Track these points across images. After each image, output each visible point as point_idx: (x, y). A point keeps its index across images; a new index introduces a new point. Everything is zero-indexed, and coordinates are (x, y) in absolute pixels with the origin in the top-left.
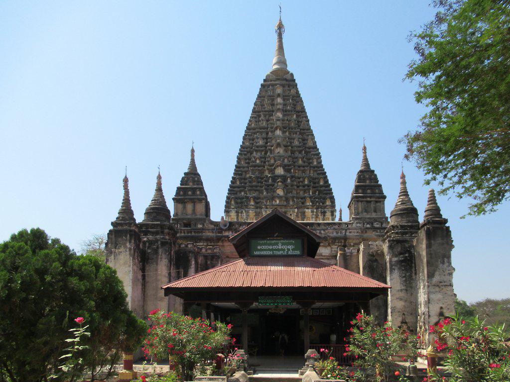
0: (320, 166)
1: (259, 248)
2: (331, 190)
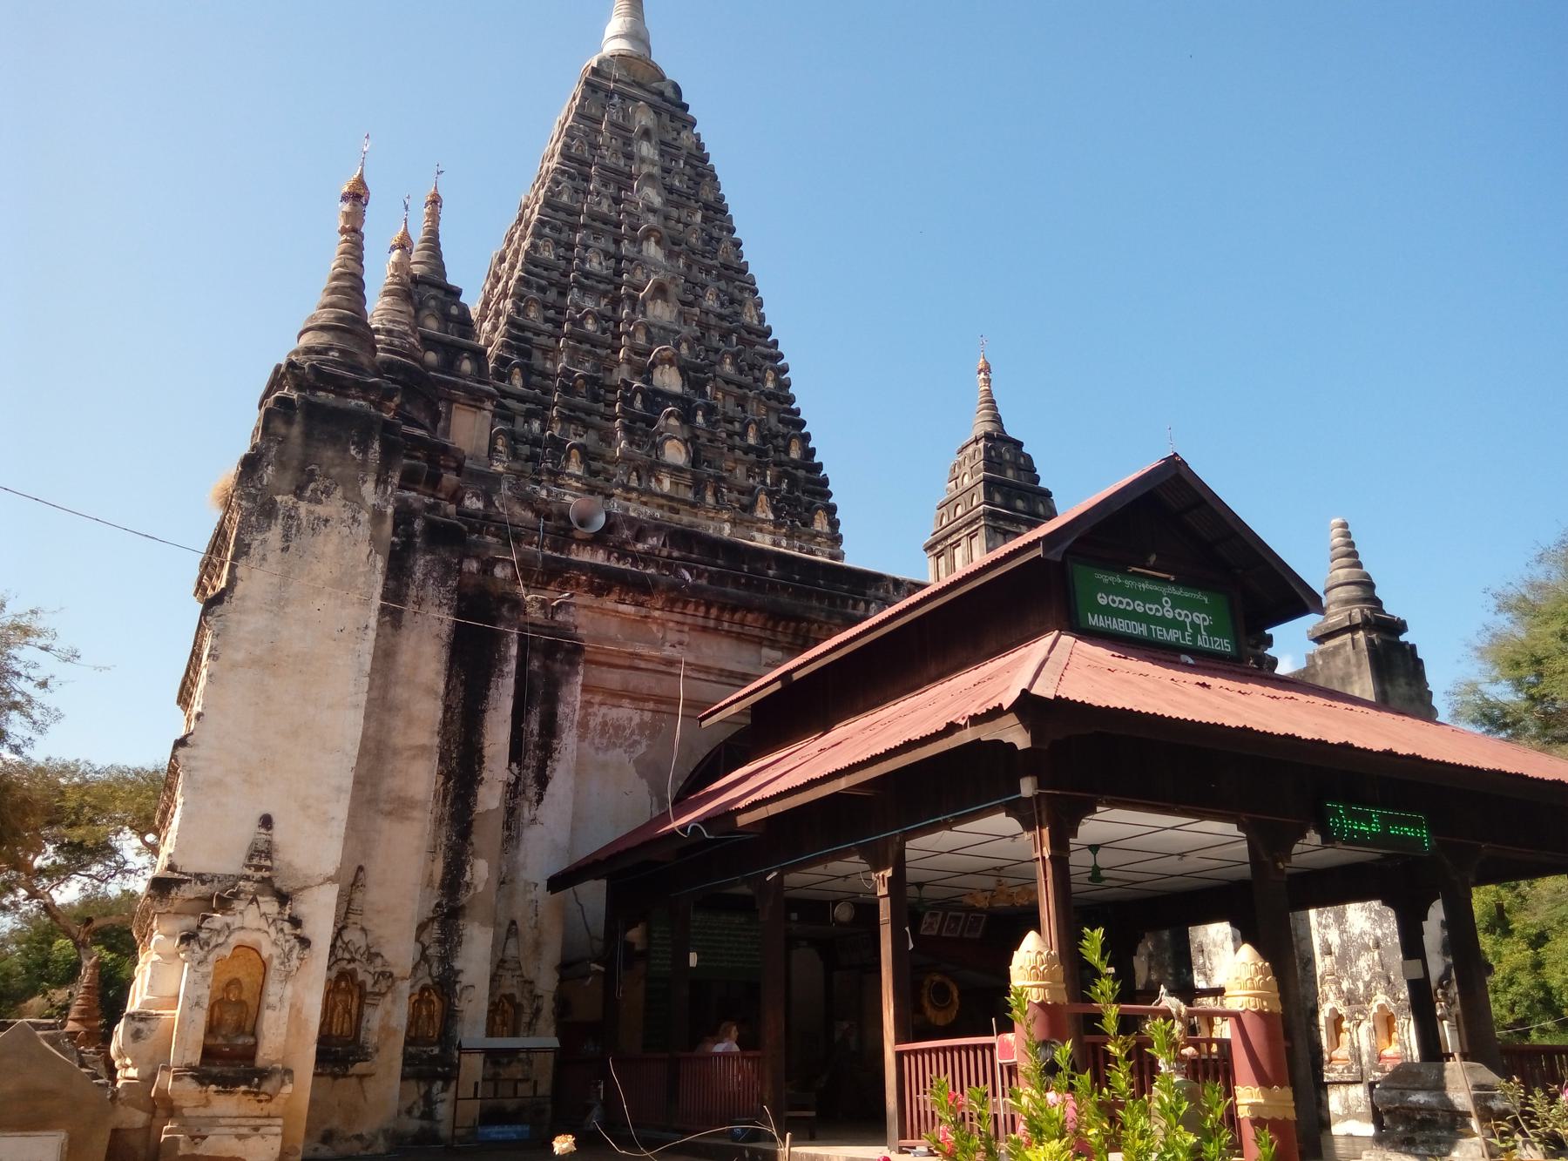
0: (782, 398)
1: (1102, 600)
2: (825, 482)
